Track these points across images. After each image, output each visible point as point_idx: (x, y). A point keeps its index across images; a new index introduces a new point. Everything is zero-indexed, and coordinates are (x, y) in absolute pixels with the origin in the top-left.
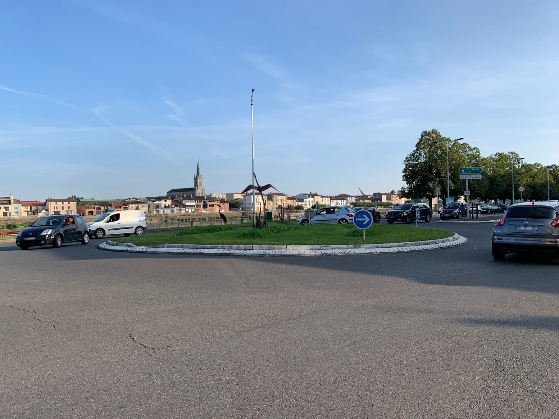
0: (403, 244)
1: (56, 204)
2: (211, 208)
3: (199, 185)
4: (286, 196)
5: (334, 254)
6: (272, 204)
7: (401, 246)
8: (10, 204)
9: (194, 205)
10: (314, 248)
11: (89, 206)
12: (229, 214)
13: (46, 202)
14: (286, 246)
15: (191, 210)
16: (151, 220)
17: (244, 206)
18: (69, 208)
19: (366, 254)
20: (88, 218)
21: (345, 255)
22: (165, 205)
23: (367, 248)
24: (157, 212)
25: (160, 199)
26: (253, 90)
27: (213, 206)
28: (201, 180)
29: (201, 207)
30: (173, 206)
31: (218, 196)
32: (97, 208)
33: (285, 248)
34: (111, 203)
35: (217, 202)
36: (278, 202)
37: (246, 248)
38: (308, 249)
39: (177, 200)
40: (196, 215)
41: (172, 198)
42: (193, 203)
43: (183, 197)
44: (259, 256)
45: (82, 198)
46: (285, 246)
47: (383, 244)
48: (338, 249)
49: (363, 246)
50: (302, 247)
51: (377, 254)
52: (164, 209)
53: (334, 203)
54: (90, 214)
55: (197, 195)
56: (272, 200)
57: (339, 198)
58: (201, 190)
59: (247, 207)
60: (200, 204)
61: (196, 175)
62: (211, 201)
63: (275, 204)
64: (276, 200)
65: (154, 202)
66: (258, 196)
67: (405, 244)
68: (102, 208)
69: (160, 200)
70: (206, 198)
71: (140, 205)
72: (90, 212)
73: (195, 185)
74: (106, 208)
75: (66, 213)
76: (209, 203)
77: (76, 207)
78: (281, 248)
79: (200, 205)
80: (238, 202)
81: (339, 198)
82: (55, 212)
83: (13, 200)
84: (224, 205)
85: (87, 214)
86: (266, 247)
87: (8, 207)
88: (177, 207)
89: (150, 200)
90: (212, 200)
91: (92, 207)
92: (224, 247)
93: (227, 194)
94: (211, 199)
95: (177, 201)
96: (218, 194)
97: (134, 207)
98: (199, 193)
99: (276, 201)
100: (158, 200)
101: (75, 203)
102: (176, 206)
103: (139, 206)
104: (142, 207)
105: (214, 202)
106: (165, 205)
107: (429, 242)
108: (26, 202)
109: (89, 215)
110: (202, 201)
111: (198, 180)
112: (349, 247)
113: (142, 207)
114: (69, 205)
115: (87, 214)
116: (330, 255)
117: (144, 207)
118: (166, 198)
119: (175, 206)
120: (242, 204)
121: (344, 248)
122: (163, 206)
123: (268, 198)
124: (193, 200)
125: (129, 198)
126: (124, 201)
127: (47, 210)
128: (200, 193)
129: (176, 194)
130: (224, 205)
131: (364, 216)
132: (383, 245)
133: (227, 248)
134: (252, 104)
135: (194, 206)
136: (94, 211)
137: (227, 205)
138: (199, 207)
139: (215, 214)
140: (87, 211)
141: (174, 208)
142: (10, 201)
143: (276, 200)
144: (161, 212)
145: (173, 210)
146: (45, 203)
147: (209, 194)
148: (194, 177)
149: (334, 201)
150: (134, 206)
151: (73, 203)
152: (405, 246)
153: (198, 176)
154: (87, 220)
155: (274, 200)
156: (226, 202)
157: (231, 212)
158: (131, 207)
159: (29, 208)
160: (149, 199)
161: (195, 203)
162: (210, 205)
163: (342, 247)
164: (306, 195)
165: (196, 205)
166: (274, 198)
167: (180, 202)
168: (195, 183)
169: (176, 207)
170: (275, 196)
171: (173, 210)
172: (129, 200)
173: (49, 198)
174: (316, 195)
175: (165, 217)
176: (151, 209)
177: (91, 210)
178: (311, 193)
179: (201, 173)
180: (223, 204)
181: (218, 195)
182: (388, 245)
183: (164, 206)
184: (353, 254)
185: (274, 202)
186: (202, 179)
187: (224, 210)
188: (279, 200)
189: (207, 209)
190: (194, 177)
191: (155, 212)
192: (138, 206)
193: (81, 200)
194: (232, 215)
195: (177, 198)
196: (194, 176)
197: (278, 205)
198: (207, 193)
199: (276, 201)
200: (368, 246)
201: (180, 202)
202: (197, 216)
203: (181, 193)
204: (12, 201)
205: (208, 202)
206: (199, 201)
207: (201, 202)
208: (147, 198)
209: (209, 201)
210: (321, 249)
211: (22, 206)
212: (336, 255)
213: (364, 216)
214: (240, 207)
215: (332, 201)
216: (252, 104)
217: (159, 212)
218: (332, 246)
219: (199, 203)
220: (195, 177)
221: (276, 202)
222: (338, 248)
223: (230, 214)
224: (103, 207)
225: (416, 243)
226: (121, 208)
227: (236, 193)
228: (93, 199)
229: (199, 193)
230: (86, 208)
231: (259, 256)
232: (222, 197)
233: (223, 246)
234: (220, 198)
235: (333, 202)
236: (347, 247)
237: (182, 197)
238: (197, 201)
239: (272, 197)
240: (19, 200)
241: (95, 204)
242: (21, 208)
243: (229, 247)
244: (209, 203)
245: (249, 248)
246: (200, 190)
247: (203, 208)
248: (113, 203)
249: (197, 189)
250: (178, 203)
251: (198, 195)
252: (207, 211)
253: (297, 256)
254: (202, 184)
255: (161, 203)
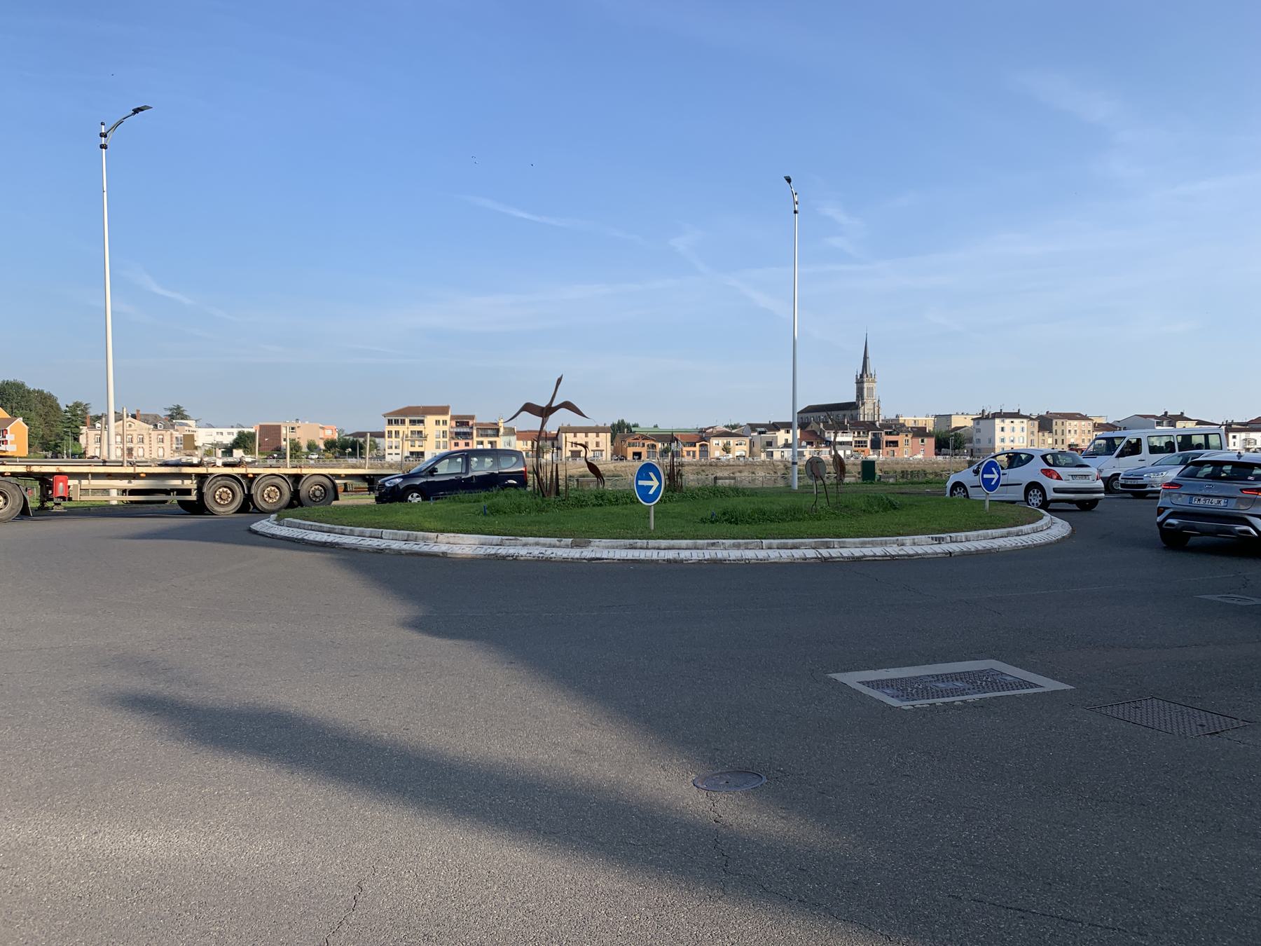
0: (708, 543)
1: (575, 436)
2: (889, 449)
3: (868, 396)
4: (1090, 422)
5: (513, 556)
6: (1050, 441)
7: (700, 547)
8: (498, 436)
9: (852, 442)
10: (487, 541)
11: (633, 441)
12: (933, 463)
13: (558, 432)
14: (436, 534)
15: (843, 451)
16: (753, 473)
17: (977, 446)
18: (597, 444)
19: (585, 561)
20: (630, 466)
21: (536, 560)
22: (787, 440)
23: (607, 548)
24: (767, 456)
25: (776, 427)
26: (789, 180)
27: (895, 443)
28: (871, 385)
29: (866, 446)
30: (804, 443)
31: (915, 421)
32: (648, 445)
33: (434, 538)
34: (678, 435)
35: (907, 436)
36: (1068, 436)
37: (373, 535)
38: (477, 543)
39: (813, 429)
40: (854, 464)
41: (803, 426)
42: (848, 438)
43: (825, 423)
44: (377, 552)
45: (635, 426)
46: (433, 535)
47: (650, 541)
48: (537, 547)
49: (596, 542)
50: (465, 539)
51: (613, 563)
52: (782, 450)
53: (1237, 440)
54: (637, 457)
55: (862, 420)
56: (1051, 432)
57: (1254, 426)
58: (872, 407)
59: (984, 448)
60: (864, 439)
61: (860, 372)
62: (890, 432)
63: (1060, 442)
64: (1063, 430)
65: (762, 435)
66: (1012, 422)
67: (713, 544)
68: (659, 445)
69: (773, 430)
70: (880, 425)
71: (733, 441)
72: (635, 454)
73: (858, 396)
74: (666, 445)
75: (592, 455)
76: (885, 438)
77: (609, 444)
78: (428, 539)
79: (865, 442)
80: (960, 435)
81: (1254, 426)
82: (572, 452)
83: (505, 428)
84: (923, 441)
85: (630, 457)
86: (403, 535)
87: (496, 442)
88: (813, 446)
89: (754, 430)
90: (894, 430)
91: (639, 443)
92: (343, 531)
93: (936, 416)
94: (890, 428)
95: (814, 433)
96: (915, 417)
97: (720, 445)
98: (866, 413)
99: (1063, 434)
100: (770, 430)
101: (609, 435)
102: (811, 443)
103: (731, 442)
104: (737, 445)
105: (898, 434)
106: (787, 440)
107: (802, 543)
108: (526, 432)
109: (634, 459)
110: (870, 433)
111: (866, 385)
112: (562, 542)
113: (737, 445)
114: (598, 439)
115: (630, 457)
116: (504, 558)
117: (741, 444)
118: (787, 426)
119: (808, 443)
120: (970, 440)
121: (550, 544)
122: (781, 442)
123: (1039, 427)
124: (849, 431)
125: (713, 427)
126: (702, 431)
127: (559, 448)
128: (868, 414)
129: (812, 416)
130: (923, 441)
131: (651, 474)
132: (648, 542)
133: (347, 532)
134: (795, 212)
135: (849, 443)
136: (644, 451)
137: (930, 442)
138: (862, 446)
139: (898, 464)
140: (630, 451)
141: (805, 447)
142: (498, 430)
143: (1063, 430)
144: (777, 455)
145: (803, 452)
146: (557, 435)
147: (894, 417)
148: (855, 378)
149: (1237, 435)
150: (720, 441)
151: (604, 434)
152: (713, 548)
153: (865, 376)
154: (627, 469)
155: (1056, 431)
156: (929, 435)
157: (940, 458)
158: (714, 444)
159: (530, 443)
160: (753, 427)
161: (854, 437)
162: (887, 442)
163: (548, 543)
164: (1153, 420)
165: (856, 441)
166: (1057, 425)
167: (819, 434)
168: (857, 392)
169: (808, 446)
170: (1059, 422)
171: (803, 452)
172: (712, 429)
173: (605, 424)
174: (1181, 417)
175: (782, 467)
176: (755, 449)
177: (637, 449)
178: (1166, 413)
179: (871, 368)
180: (920, 440)
181: (915, 419)
182: (664, 543)
183: (784, 442)
184: (553, 559)
185: (1056, 437)
186: (875, 382)
187: (922, 453)
188: (1070, 431)
189: (881, 451)
190: (857, 378)
191: (763, 456)
192: (728, 443)
193: (633, 429)
194: (943, 466)
195: (813, 427)
196: (857, 376)
197: (1067, 443)
198: (887, 414)
199: (1063, 434)
200: (610, 544)
201: (819, 434)
202: (855, 467)
203: (822, 415)
204: (502, 430)
205: (883, 433)
206: (861, 433)
207: (868, 434)
208: (749, 424)
209: (886, 433)
210: (501, 545)
211: (518, 439)
212: (515, 559)
213: (651, 474)
214: (964, 448)
215: (1231, 435)
216: (795, 212)
217: (772, 456)
218: (524, 539)
219: (863, 437)
220: (859, 377)
221: (1063, 437)
222: (537, 544)
223: (937, 463)
224: (660, 444)
225: (753, 542)
226: (695, 446)
227: (957, 414)
228: (656, 426)
229: (866, 413)
230: (629, 445)
231: (377, 552)
232: (924, 422)
233: (342, 529)
234: (920, 426)
235: (1234, 437)
236: (558, 543)
237: (823, 422)
238: (859, 433)
239: (1052, 423)
240: (514, 429)
241: (646, 438)
242: (515, 444)
243: (351, 530)
244: (885, 438)
245: (377, 535)
246: (868, 407)
247: (872, 448)
248: (681, 435)
249: (863, 404)
250: (814, 437)
251: (864, 418)
252: (881, 455)
253: (439, 556)
254: (874, 394)
255: (777, 437)
